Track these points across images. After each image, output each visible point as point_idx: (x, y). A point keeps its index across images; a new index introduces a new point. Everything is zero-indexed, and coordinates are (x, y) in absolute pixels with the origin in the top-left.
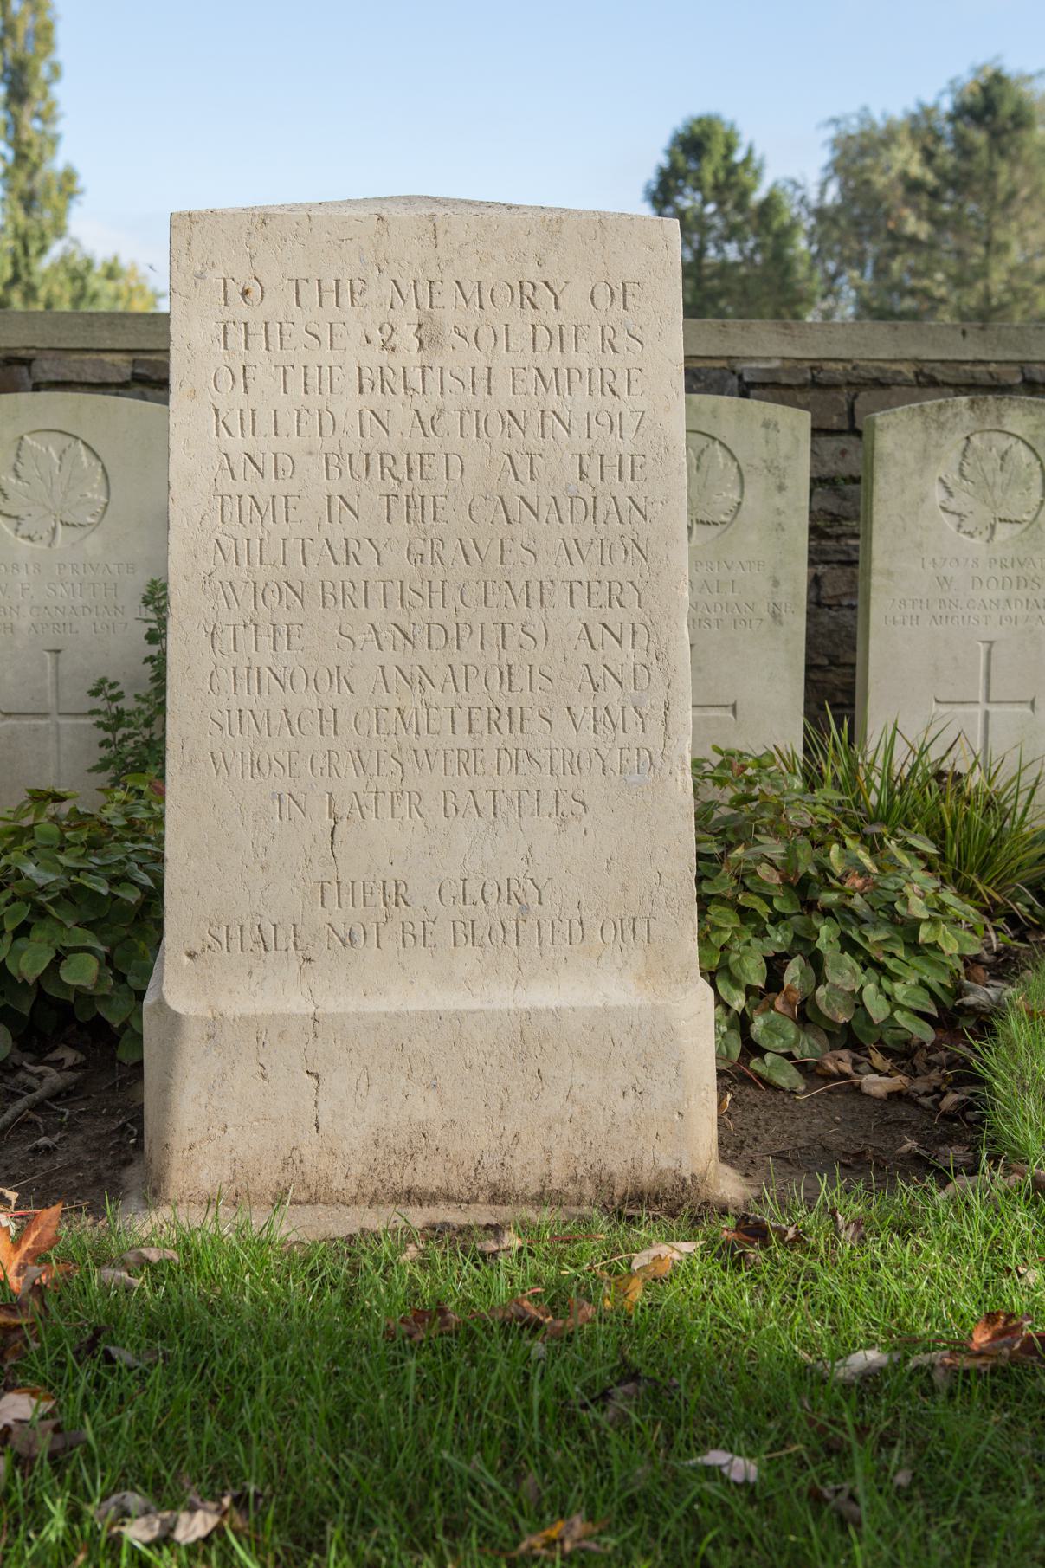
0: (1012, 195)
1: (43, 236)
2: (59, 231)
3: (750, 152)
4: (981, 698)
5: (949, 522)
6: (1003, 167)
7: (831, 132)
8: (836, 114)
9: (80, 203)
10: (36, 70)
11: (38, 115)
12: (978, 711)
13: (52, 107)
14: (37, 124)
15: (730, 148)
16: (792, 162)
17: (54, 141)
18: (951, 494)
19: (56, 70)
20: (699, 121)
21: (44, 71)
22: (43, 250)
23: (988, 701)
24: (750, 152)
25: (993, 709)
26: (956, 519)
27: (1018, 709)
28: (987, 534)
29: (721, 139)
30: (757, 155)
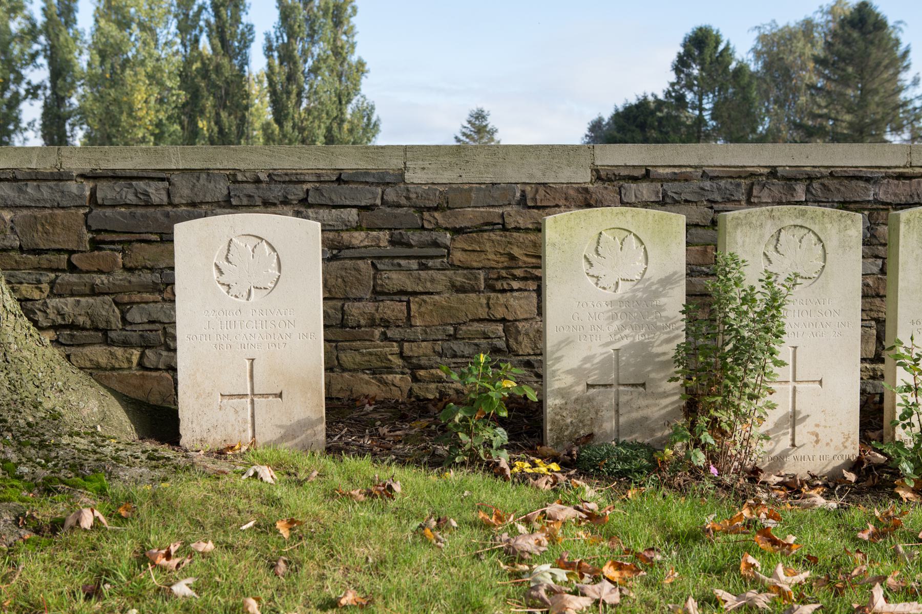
0: (878, 64)
1: (349, 94)
2: (357, 90)
3: (728, 44)
4: (791, 379)
5: (591, 281)
6: (873, 50)
7: (756, 34)
8: (759, 25)
9: (876, 8)
10: (346, 10)
11: (345, 33)
12: (790, 387)
13: (352, 28)
14: (344, 38)
15: (718, 42)
16: (743, 48)
17: (353, 46)
18: (591, 265)
19: (355, 10)
20: (701, 29)
21: (349, 10)
22: (349, 101)
23: (794, 380)
24: (728, 44)
25: (797, 386)
26: (595, 280)
27: (811, 385)
28: (613, 288)
29: (714, 38)
30: (731, 46)
